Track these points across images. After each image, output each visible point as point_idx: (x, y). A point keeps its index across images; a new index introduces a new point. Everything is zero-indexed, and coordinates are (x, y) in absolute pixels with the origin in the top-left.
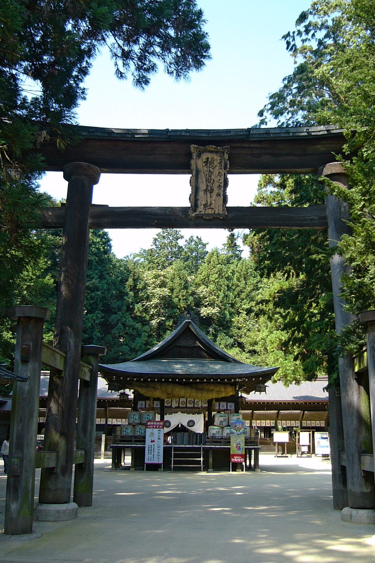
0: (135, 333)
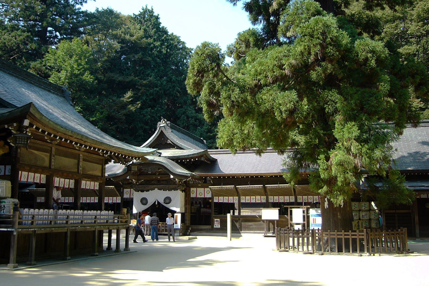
0: (197, 123)
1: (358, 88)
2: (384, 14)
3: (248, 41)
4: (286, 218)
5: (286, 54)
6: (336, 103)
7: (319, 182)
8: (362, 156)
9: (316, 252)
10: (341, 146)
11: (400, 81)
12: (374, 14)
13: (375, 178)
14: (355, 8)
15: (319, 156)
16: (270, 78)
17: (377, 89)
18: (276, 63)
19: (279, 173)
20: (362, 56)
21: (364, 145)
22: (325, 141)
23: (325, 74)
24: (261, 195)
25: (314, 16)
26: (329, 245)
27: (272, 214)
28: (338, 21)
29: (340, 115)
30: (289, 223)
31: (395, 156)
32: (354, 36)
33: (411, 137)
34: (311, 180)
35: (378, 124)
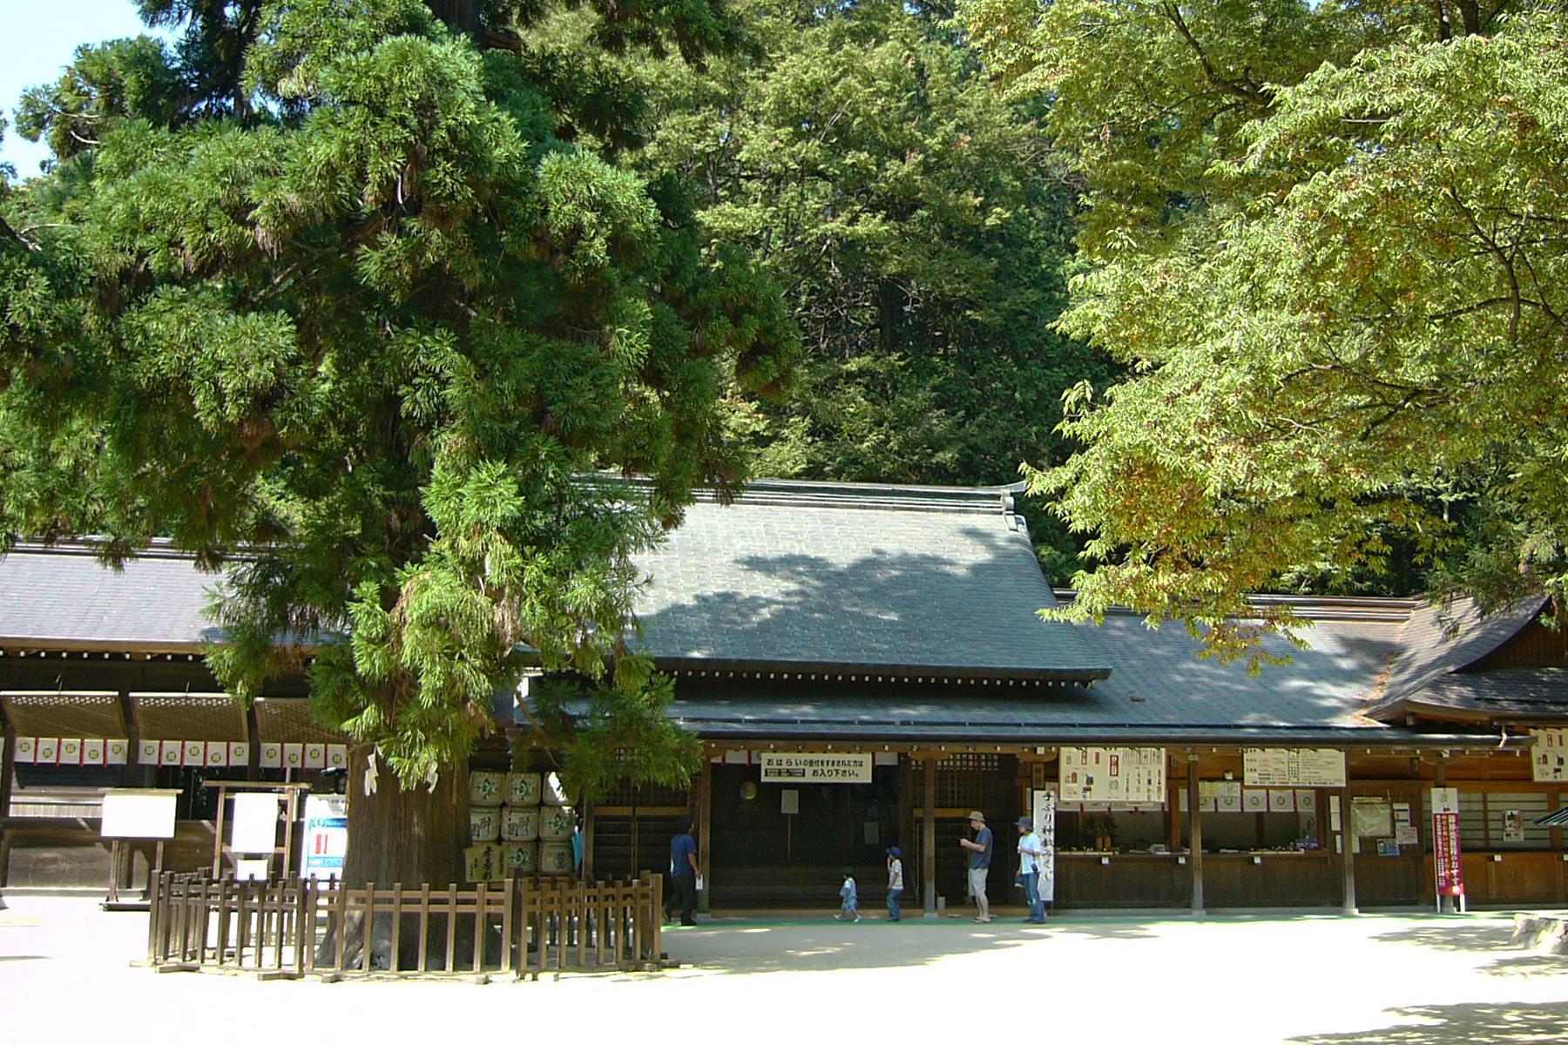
1: (533, 337)
2: (663, 75)
3: (119, 88)
4: (206, 830)
5: (267, 165)
6: (444, 384)
7: (350, 689)
8: (523, 598)
9: (313, 973)
10: (448, 553)
11: (692, 328)
12: (629, 68)
13: (565, 682)
14: (562, 32)
15: (356, 584)
16: (188, 252)
17: (604, 346)
18: (220, 192)
19: (195, 644)
20: (562, 214)
21: (533, 555)
22: (389, 528)
23: (416, 266)
24: (105, 732)
25: (398, 33)
26: (367, 943)
27: (145, 815)
28: (486, 69)
29: (454, 431)
30: (217, 853)
31: (646, 605)
32: (539, 138)
33: (714, 538)
34: (318, 679)
35: (593, 480)
